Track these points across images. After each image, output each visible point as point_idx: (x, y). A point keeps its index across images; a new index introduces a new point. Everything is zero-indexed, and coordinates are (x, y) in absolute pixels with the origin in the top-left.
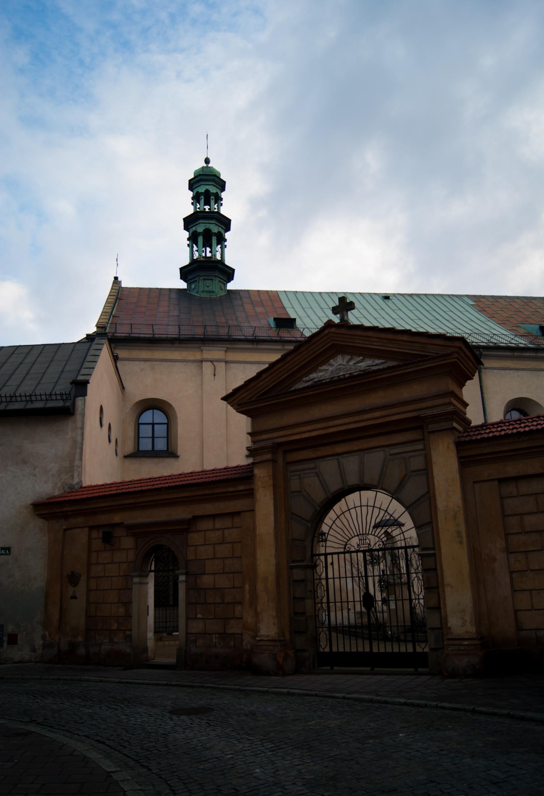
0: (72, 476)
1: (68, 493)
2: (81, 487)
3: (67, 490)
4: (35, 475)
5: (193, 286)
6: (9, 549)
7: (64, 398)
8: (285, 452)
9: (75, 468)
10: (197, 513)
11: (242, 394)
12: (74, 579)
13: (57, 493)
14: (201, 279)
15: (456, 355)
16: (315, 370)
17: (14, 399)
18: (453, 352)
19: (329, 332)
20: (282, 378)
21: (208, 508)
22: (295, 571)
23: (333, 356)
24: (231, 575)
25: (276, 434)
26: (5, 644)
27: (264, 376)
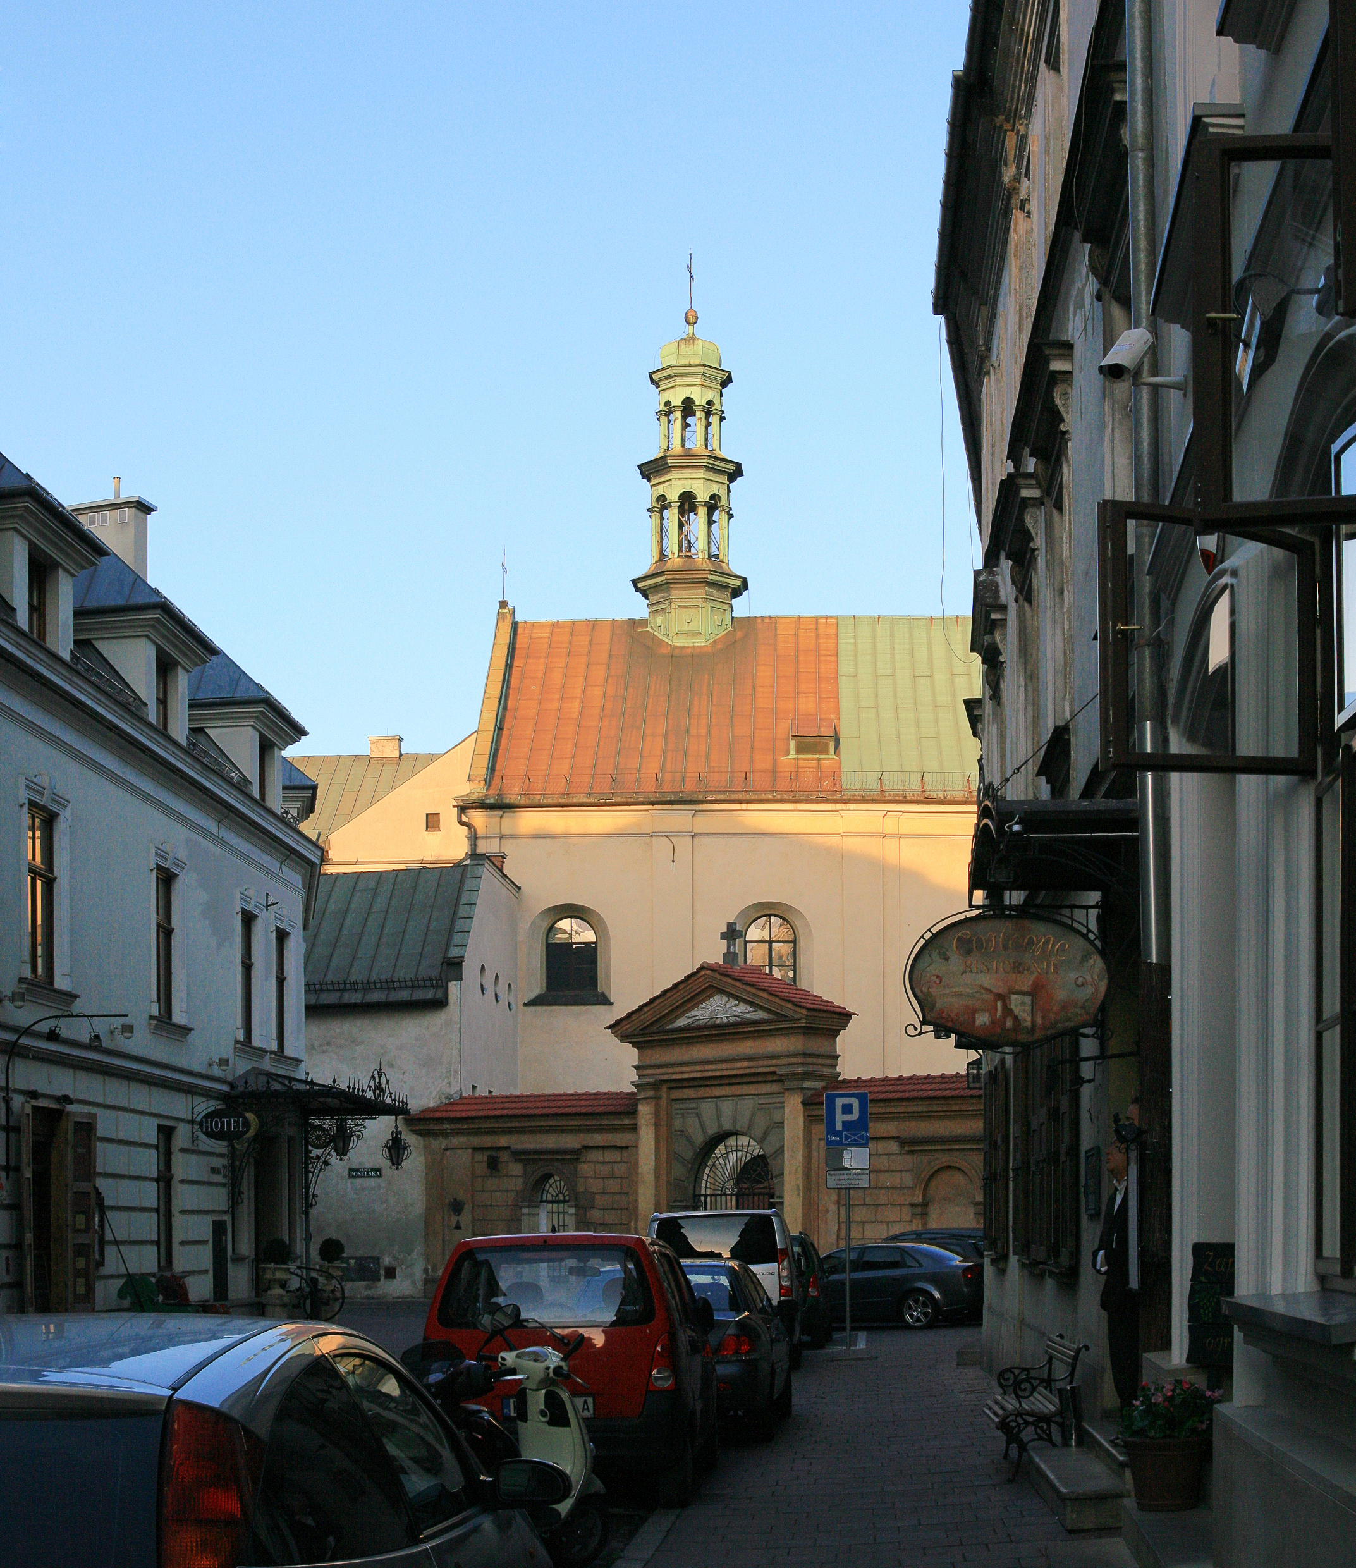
2: (461, 1097)
3: (445, 1101)
5: (659, 620)
6: (380, 1170)
8: (671, 1088)
10: (585, 1143)
12: (457, 1207)
14: (673, 606)
21: (598, 1139)
24: (619, 1212)
25: (658, 1071)
26: (382, 1278)
27: (645, 1009)
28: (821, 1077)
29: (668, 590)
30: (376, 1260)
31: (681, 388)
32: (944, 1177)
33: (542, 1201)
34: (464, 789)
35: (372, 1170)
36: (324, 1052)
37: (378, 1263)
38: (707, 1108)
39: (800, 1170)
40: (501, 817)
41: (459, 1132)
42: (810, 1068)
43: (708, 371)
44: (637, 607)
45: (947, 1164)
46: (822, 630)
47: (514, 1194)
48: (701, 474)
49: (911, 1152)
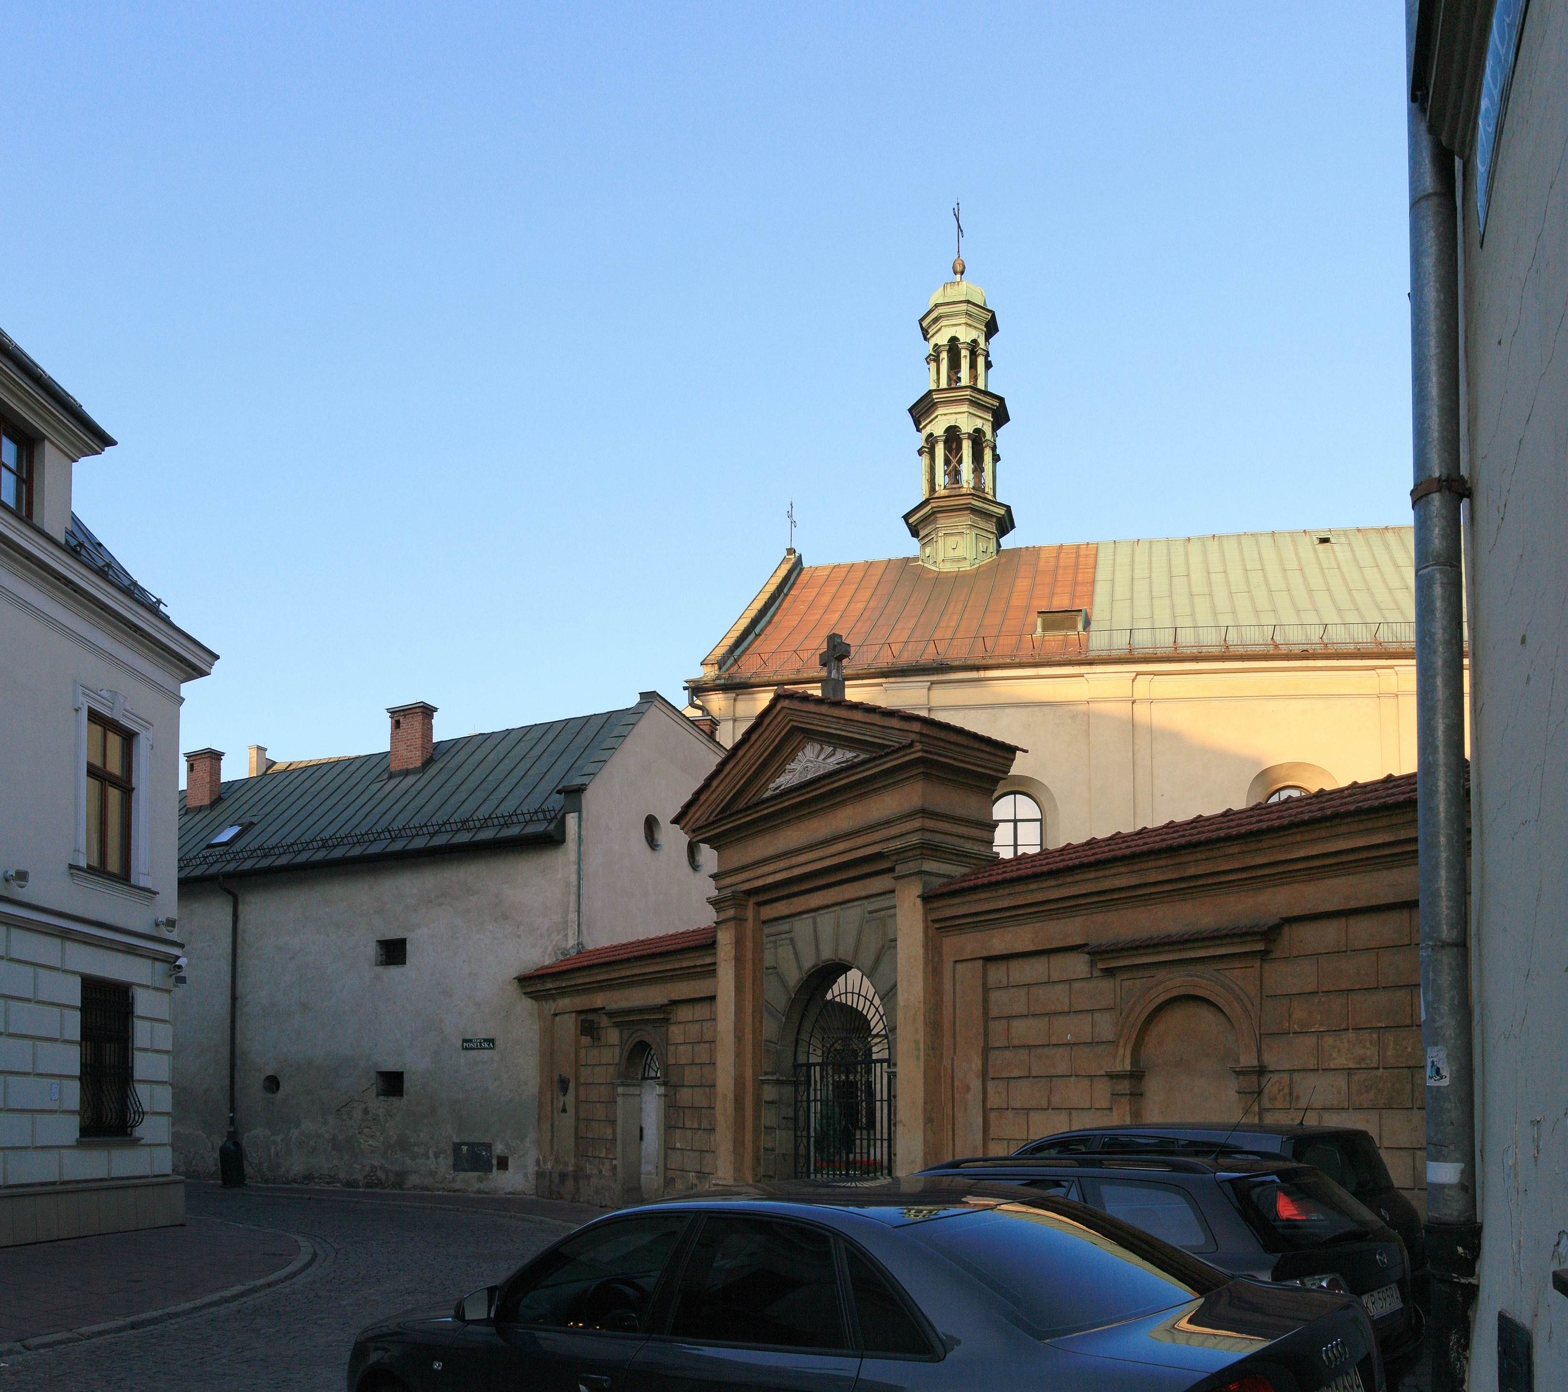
0: (566, 936)
1: (562, 961)
3: (561, 958)
4: (519, 936)
6: (492, 1041)
7: (549, 817)
8: (759, 904)
9: (569, 924)
10: (675, 997)
11: (695, 813)
12: (564, 1085)
13: (547, 962)
14: (940, 534)
15: (918, 746)
16: (780, 771)
17: (514, 818)
18: (913, 742)
19: (783, 708)
20: (738, 786)
22: (766, 1087)
23: (800, 747)
26: (495, 1169)
28: (960, 856)
29: (935, 521)
30: (488, 1147)
31: (947, 329)
32: (1176, 1018)
33: (644, 1078)
34: (699, 673)
35: (485, 1040)
36: (440, 905)
37: (491, 1151)
38: (802, 927)
39: (920, 1017)
40: (735, 700)
41: (562, 992)
42: (937, 838)
43: (972, 309)
44: (910, 547)
45: (1182, 991)
46: (1082, 552)
47: (612, 1067)
48: (965, 408)
49: (1109, 972)
